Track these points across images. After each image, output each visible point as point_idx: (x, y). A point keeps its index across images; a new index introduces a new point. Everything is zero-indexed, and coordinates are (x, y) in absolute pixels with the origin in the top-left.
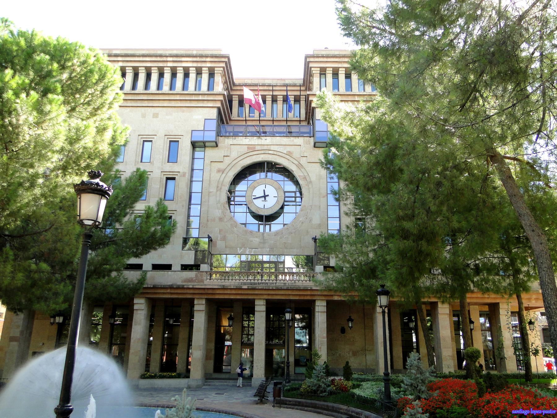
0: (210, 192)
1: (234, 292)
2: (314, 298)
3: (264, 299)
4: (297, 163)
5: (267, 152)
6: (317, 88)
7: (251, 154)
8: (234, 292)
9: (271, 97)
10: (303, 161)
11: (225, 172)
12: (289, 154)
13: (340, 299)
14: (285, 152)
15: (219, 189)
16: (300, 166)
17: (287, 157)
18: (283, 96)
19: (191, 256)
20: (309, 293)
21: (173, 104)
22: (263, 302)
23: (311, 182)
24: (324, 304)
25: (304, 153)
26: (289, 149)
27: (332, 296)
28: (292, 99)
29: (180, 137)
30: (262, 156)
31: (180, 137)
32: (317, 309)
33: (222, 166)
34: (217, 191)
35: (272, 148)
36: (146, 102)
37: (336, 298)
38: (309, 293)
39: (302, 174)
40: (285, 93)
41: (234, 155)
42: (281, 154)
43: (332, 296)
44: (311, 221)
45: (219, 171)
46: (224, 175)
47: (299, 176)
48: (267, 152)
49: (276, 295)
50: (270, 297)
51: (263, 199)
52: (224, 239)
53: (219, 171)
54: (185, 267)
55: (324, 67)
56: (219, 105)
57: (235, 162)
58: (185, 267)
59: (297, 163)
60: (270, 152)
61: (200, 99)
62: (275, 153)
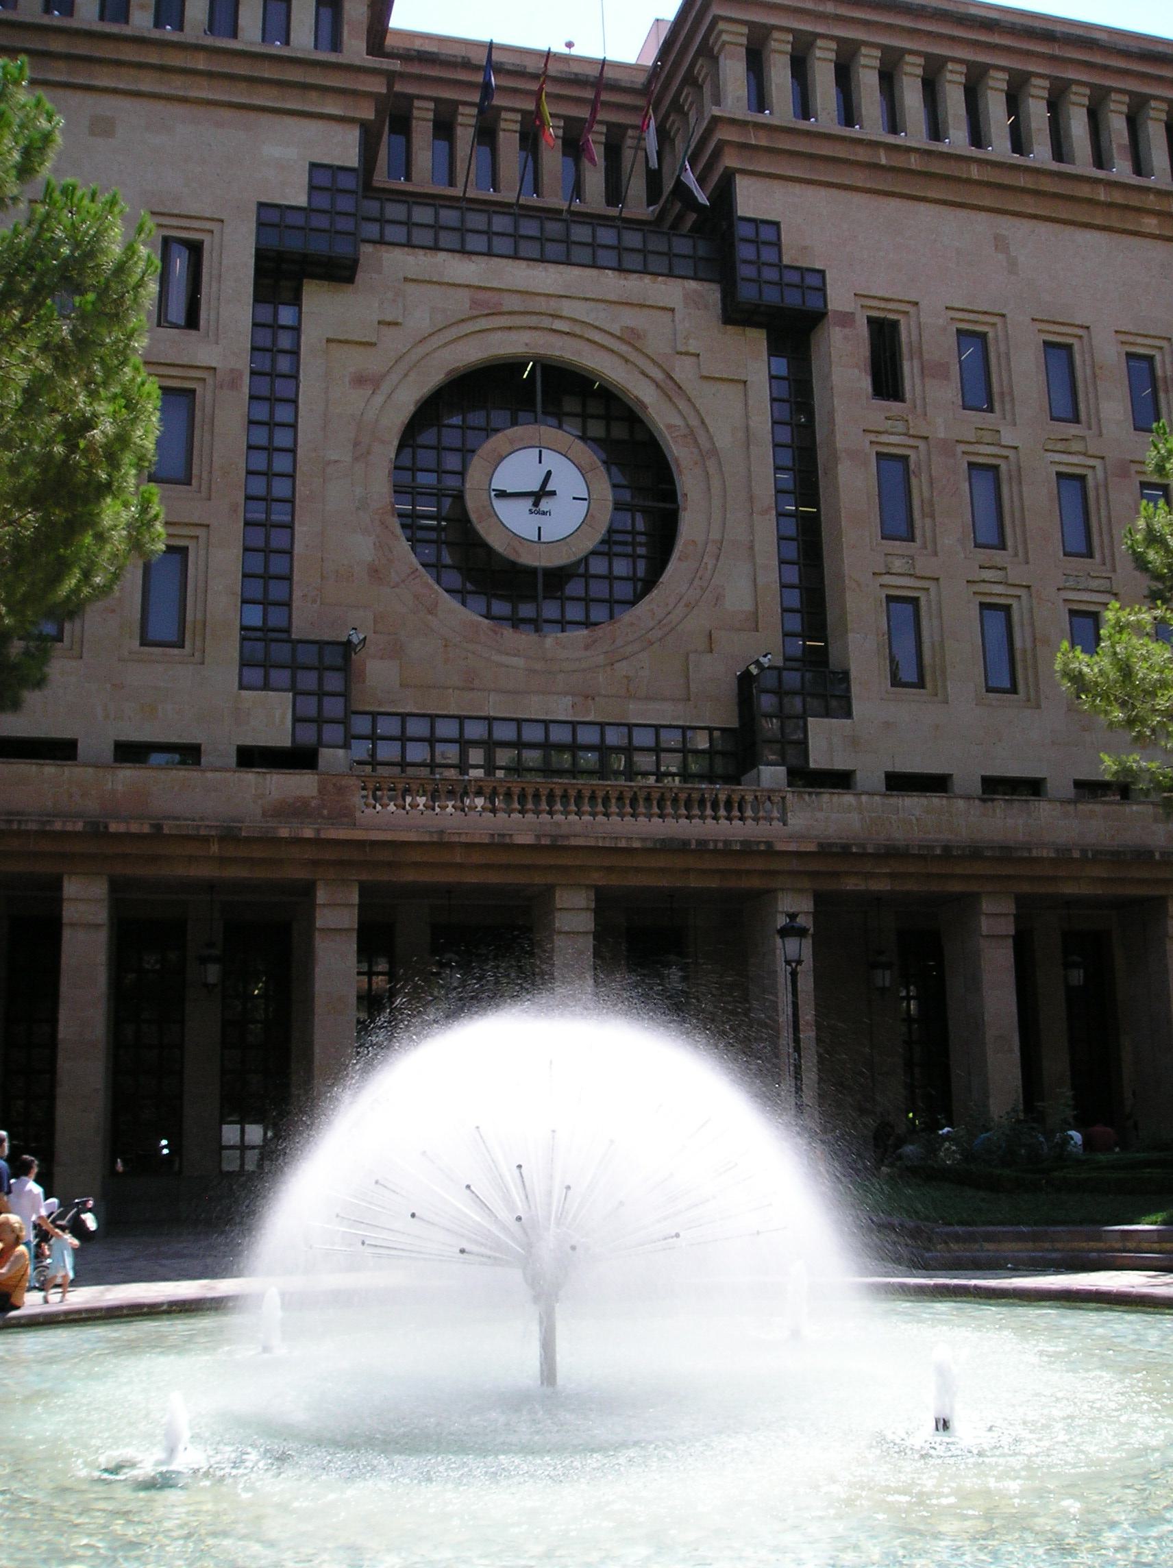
0: (329, 463)
1: (477, 858)
2: (974, 887)
3: (588, 887)
4: (658, 375)
5: (546, 322)
6: (739, 99)
7: (483, 323)
8: (477, 858)
9: (475, 111)
10: (684, 371)
11: (386, 387)
12: (631, 337)
13: (862, 887)
14: (615, 329)
15: (361, 453)
16: (671, 388)
17: (623, 349)
18: (524, 113)
19: (278, 714)
20: (760, 865)
21: (176, 86)
22: (99, 889)
23: (714, 452)
24: (1009, 907)
25: (687, 338)
26: (630, 318)
27: (836, 875)
28: (553, 131)
29: (208, 225)
30: (526, 336)
31: (208, 225)
32: (324, 918)
33: (372, 362)
34: (356, 459)
35: (568, 308)
36: (61, 65)
37: (852, 884)
38: (760, 865)
39: (678, 421)
40: (530, 106)
41: (419, 320)
42: (598, 337)
43: (836, 875)
44: (719, 599)
45: (360, 380)
46: (379, 399)
47: (669, 427)
48: (546, 322)
49: (637, 870)
50: (614, 880)
51: (528, 503)
52: (396, 651)
53: (360, 380)
54: (250, 757)
55: (764, 26)
56: (368, 113)
57: (421, 350)
58: (250, 757)
59: (658, 375)
60: (558, 325)
61: (145, 87)
62: (577, 329)
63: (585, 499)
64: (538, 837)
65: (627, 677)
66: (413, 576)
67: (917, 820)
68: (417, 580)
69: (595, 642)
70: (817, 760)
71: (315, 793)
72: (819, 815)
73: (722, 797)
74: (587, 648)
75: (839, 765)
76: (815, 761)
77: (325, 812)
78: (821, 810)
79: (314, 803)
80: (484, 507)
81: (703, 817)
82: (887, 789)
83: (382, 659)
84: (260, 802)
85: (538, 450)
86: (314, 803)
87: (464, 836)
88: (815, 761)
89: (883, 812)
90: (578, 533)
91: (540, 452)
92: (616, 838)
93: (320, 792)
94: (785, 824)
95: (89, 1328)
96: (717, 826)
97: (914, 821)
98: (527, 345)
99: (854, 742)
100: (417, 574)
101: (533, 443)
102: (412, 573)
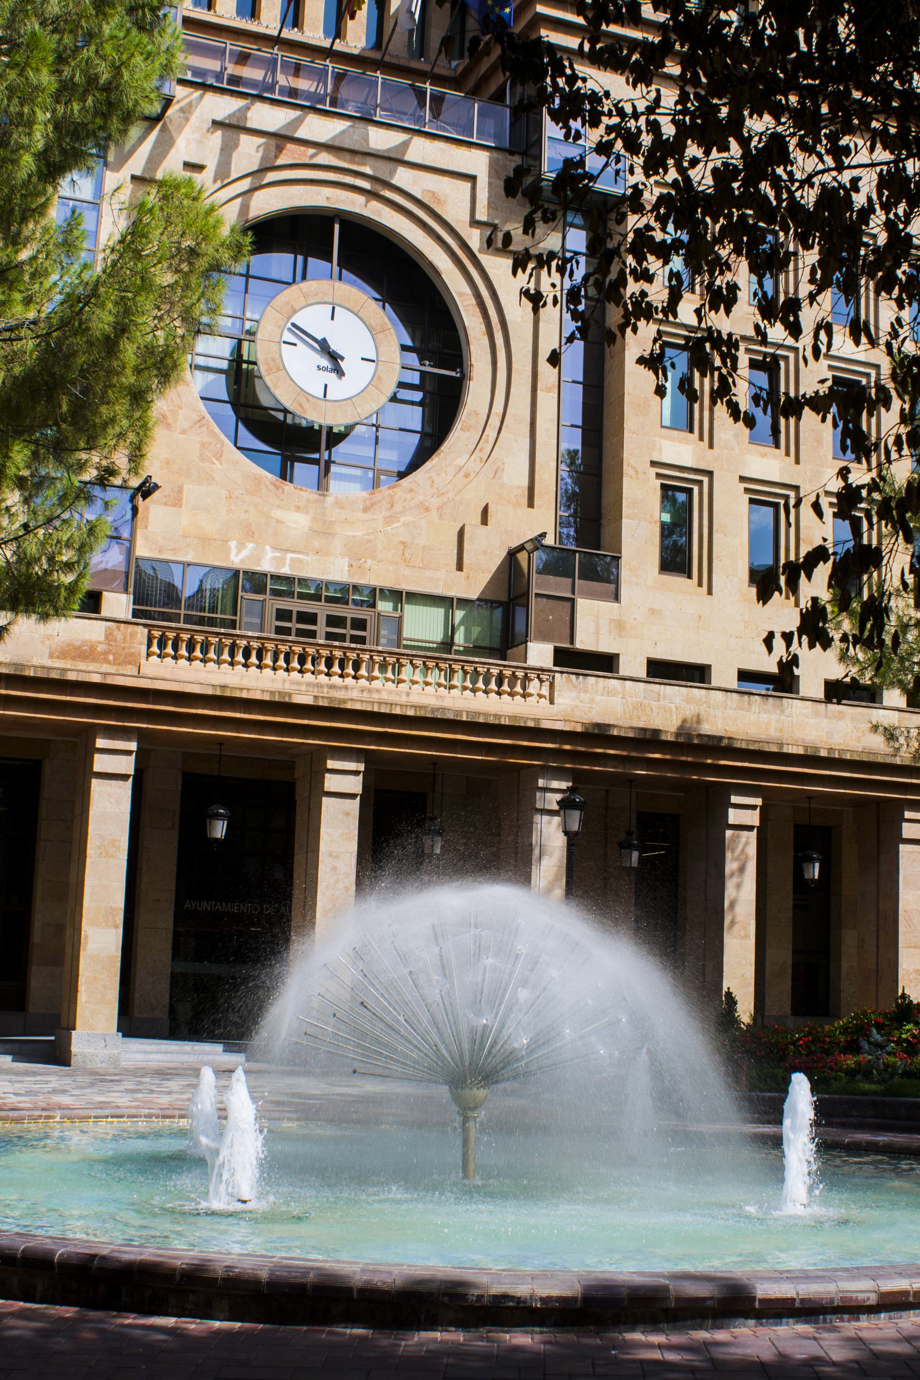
63: (373, 361)
64: (316, 697)
65: (403, 543)
66: (199, 424)
67: (677, 708)
68: (204, 428)
69: (373, 505)
70: (584, 641)
71: (102, 638)
72: (583, 696)
73: (495, 671)
74: (365, 510)
75: (605, 646)
76: (581, 642)
77: (111, 657)
78: (586, 692)
79: (100, 648)
80: (274, 360)
81: (512, 694)
82: (908, 705)
83: (165, 504)
84: (48, 643)
85: (331, 307)
86: (100, 648)
87: (398, 707)
88: (581, 642)
89: (645, 697)
90: (364, 393)
91: (334, 308)
92: (391, 704)
93: (107, 637)
94: (552, 702)
95: (440, 1275)
96: (487, 700)
97: (674, 710)
98: (327, 198)
99: (620, 626)
100: (204, 421)
101: (326, 299)
102: (199, 421)
